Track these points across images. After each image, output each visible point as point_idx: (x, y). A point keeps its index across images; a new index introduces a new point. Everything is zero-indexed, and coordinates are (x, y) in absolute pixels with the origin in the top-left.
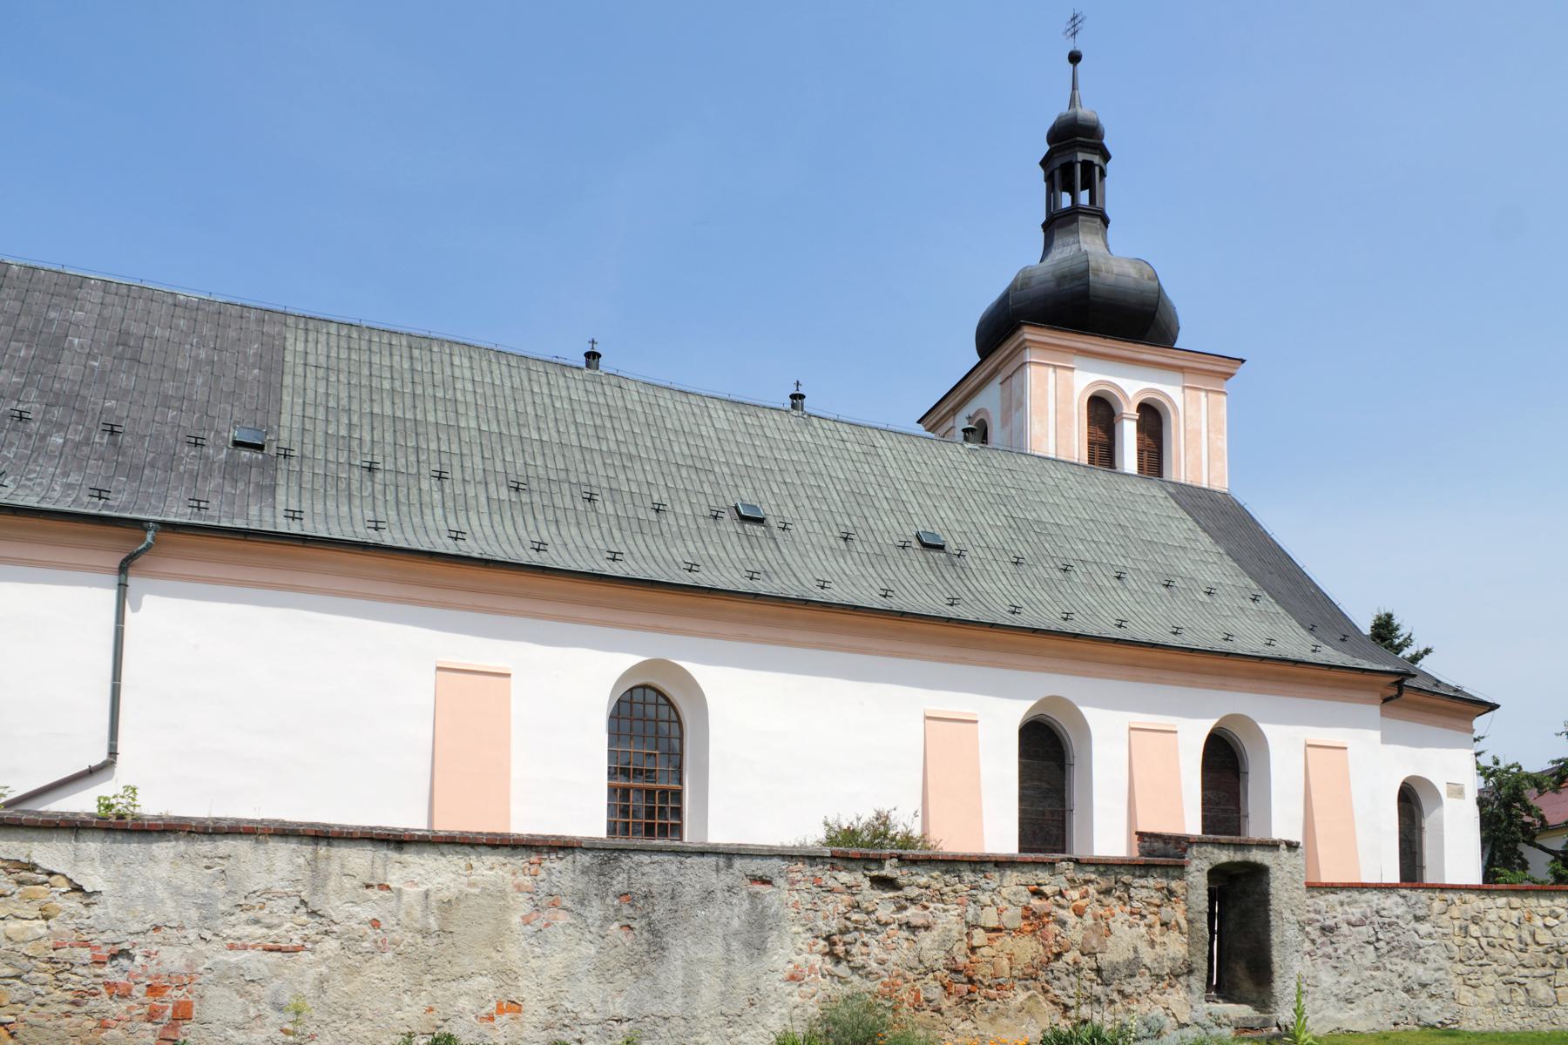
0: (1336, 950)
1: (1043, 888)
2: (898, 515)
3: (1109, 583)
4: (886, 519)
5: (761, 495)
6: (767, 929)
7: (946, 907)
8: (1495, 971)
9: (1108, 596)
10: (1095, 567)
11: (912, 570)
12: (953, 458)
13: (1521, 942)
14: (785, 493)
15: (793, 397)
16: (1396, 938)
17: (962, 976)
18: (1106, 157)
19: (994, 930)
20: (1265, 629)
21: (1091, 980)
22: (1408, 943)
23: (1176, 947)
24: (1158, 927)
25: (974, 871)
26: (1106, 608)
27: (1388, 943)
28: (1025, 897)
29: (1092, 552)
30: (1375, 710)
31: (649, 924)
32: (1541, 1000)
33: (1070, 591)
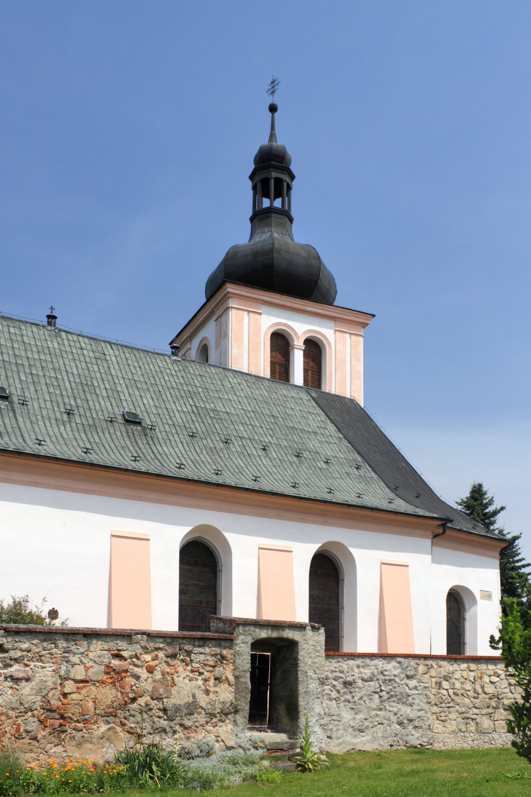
0: (353, 697)
1: (122, 653)
2: (112, 400)
4: (102, 402)
5: (11, 381)
7: (43, 665)
8: (457, 711)
9: (254, 461)
10: (249, 441)
11: (114, 437)
12: (161, 365)
13: (475, 692)
14: (30, 380)
15: (49, 317)
16: (393, 690)
17: (56, 713)
19: (82, 681)
20: (361, 487)
21: (159, 717)
22: (401, 693)
24: (212, 681)
25: (67, 640)
26: (250, 468)
27: (388, 693)
28: (107, 658)
29: (249, 432)
30: (428, 542)
32: (485, 729)
33: (227, 456)
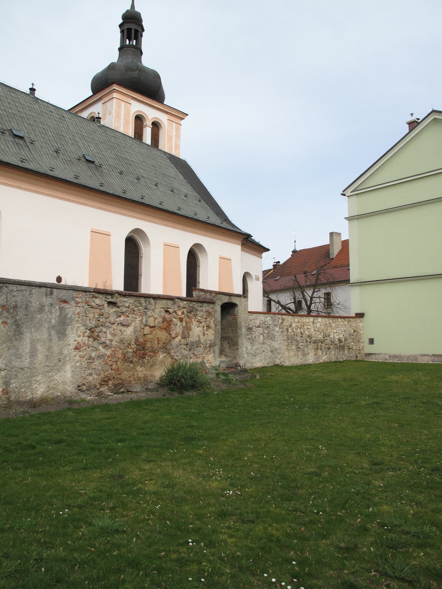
2: (75, 146)
3: (153, 187)
6: (67, 325)
15: (31, 89)
18: (143, 30)
19: (152, 327)
23: (211, 335)
31: (15, 322)
